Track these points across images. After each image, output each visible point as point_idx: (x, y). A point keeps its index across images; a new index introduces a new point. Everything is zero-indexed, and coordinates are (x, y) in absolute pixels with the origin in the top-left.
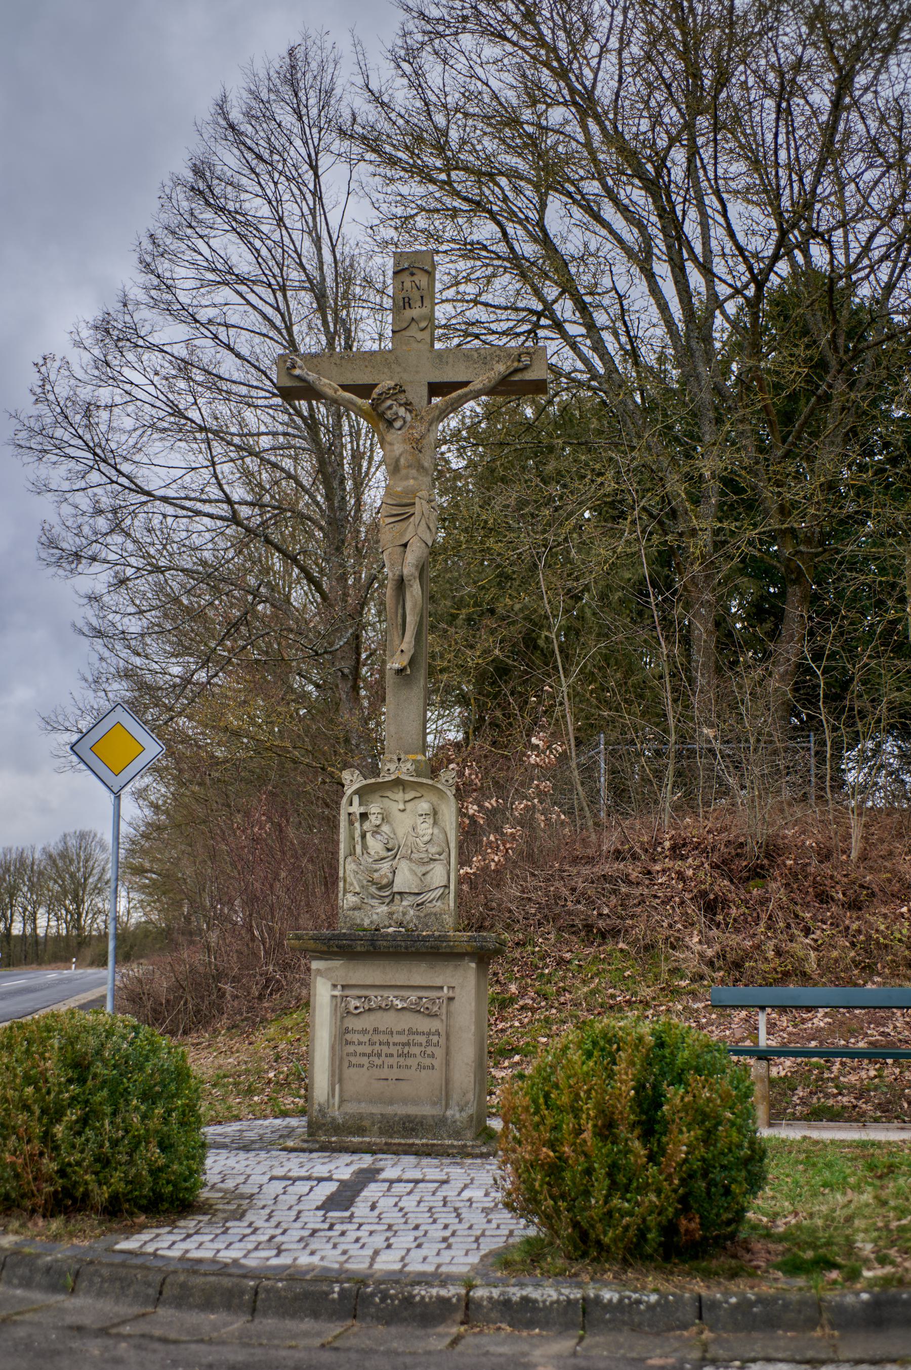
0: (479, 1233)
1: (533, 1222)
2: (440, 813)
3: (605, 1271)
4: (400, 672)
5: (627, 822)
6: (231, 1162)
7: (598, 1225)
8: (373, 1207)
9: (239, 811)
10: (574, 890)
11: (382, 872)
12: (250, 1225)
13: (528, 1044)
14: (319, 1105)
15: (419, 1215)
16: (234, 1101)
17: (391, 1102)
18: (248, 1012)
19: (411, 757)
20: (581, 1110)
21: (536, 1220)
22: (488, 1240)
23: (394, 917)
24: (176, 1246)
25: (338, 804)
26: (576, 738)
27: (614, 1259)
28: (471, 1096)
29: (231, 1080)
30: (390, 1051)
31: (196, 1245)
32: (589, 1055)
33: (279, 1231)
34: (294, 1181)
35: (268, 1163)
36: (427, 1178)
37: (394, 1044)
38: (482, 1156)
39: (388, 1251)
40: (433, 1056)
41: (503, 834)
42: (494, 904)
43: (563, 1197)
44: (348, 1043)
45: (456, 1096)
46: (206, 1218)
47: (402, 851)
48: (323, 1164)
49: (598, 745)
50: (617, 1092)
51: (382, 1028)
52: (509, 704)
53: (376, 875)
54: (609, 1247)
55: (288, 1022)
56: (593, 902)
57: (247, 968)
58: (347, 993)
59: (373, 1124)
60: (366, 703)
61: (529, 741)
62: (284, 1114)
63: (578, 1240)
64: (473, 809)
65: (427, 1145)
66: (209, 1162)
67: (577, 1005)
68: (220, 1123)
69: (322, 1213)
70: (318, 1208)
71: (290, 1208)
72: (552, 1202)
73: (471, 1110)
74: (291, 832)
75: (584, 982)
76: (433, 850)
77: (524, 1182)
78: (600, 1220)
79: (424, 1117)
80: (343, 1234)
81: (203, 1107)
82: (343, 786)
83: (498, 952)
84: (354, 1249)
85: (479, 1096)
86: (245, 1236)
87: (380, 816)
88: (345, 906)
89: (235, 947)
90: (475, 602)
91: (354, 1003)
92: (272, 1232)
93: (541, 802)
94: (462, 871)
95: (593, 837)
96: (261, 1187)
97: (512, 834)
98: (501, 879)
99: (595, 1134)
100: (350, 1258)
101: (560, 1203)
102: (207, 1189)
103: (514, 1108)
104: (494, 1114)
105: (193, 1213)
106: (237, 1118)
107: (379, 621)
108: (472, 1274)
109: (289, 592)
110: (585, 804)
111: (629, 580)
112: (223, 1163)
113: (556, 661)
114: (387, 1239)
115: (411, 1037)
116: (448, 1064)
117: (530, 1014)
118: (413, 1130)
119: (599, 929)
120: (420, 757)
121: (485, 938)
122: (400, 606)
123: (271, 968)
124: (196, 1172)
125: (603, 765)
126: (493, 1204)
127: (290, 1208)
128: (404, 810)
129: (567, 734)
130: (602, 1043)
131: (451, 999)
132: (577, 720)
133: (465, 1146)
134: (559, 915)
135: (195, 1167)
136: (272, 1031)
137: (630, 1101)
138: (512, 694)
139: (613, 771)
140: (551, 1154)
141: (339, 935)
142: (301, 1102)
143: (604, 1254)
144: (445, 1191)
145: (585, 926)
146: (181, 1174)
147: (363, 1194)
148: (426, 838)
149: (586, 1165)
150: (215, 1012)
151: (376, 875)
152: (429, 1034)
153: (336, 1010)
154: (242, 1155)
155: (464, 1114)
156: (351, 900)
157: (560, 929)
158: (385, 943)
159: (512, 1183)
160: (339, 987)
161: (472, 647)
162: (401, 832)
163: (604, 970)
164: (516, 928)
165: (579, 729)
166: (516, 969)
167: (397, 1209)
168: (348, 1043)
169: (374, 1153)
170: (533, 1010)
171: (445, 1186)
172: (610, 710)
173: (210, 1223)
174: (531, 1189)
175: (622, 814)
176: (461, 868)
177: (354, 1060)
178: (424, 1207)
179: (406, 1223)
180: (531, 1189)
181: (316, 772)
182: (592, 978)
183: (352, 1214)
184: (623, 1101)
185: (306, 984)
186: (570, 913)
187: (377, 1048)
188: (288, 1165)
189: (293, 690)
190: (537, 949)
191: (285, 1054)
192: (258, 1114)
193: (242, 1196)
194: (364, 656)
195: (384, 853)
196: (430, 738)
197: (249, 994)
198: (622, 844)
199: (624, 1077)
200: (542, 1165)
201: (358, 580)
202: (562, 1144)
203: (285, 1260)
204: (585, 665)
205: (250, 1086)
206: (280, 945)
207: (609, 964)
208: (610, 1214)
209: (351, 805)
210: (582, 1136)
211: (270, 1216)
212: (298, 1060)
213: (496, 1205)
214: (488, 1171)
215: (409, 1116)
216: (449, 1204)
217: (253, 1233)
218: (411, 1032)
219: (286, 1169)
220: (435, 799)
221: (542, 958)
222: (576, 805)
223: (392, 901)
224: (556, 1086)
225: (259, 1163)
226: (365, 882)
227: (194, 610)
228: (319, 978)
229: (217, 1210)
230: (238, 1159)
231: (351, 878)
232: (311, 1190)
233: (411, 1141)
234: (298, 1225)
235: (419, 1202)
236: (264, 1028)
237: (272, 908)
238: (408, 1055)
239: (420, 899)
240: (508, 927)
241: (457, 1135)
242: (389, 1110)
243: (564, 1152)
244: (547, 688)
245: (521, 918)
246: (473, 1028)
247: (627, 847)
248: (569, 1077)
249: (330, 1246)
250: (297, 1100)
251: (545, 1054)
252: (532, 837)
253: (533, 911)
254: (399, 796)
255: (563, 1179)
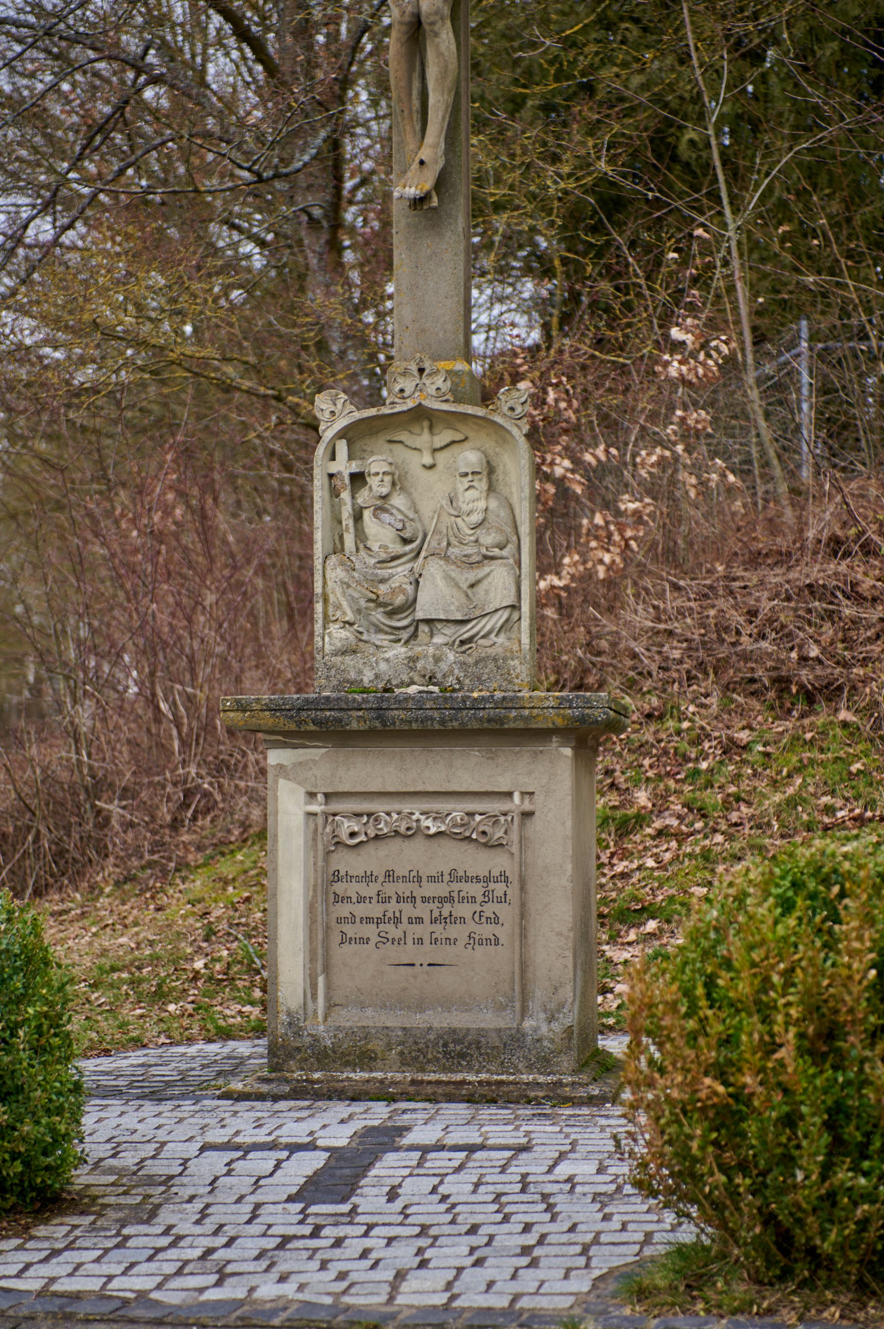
0: (589, 1238)
1: (688, 1216)
2: (500, 471)
3: (826, 1305)
4: (418, 203)
5: (853, 485)
6: (130, 1121)
7: (810, 1219)
8: (392, 1195)
9: (124, 485)
10: (752, 613)
11: (395, 583)
12: (166, 1232)
13: (671, 899)
14: (289, 1014)
15: (478, 1208)
16: (130, 1012)
17: (421, 1008)
18: (152, 852)
19: (443, 365)
20: (775, 1008)
21: (694, 1211)
22: (606, 1250)
23: (419, 665)
24: (31, 1272)
25: (308, 463)
26: (754, 329)
27: (842, 1282)
28: (567, 993)
29: (125, 975)
30: (416, 913)
31: (69, 1269)
32: (787, 906)
33: (221, 1240)
34: (247, 1153)
35: (198, 1120)
36: (490, 1142)
37: (425, 900)
38: (591, 1101)
39: (422, 1273)
40: (495, 920)
41: (618, 513)
42: (604, 644)
43: (743, 1167)
44: (339, 899)
45: (539, 994)
46: (87, 1220)
47: (432, 543)
48: (298, 1120)
49: (793, 344)
50: (845, 972)
51: (401, 872)
52: (628, 265)
53: (383, 589)
54: (830, 1259)
55: (226, 868)
56: (790, 635)
57: (148, 772)
58: (335, 807)
59: (389, 1047)
60: (355, 276)
61: (666, 336)
62: (225, 1035)
63: (774, 1249)
64: (562, 467)
65: (489, 1083)
66: (88, 1121)
67: (762, 826)
68: (107, 1053)
69: (299, 1206)
70: (290, 1199)
71: (239, 1200)
72: (723, 1179)
73: (570, 1018)
74: (221, 520)
75: (774, 784)
76: (488, 539)
77: (670, 1142)
78: (815, 1210)
79: (482, 1032)
80: (338, 1243)
81: (74, 1025)
82: (316, 428)
83: (614, 727)
84: (359, 1270)
85: (584, 994)
86: (158, 1250)
87: (388, 479)
88: (328, 648)
89: (125, 734)
90: (560, 70)
91: (348, 825)
92: (209, 1242)
93: (688, 450)
94: (543, 585)
95: (789, 514)
96: (185, 1162)
97: (636, 512)
98: (616, 597)
99: (801, 1052)
100: (351, 1285)
101: (738, 1180)
102: (87, 1168)
103: (651, 1006)
104: (611, 1028)
105: (62, 1213)
106: (139, 1043)
107: (377, 118)
108: (577, 1311)
109: (203, 66)
110: (772, 453)
111: (856, 18)
112: (114, 1122)
113: (716, 180)
114: (420, 1251)
115: (456, 886)
116: (523, 934)
117: (674, 844)
118: (462, 1055)
119: (802, 686)
120: (460, 366)
121: (588, 700)
122: (416, 76)
123: (193, 770)
124: (66, 1136)
125: (806, 378)
126: (613, 1187)
127: (239, 1200)
128: (432, 467)
129: (737, 322)
130: (812, 885)
131: (527, 815)
132: (756, 295)
133: (559, 1084)
134: (727, 660)
135: (62, 1128)
136: (198, 884)
137: (867, 988)
138: (632, 245)
139: (825, 390)
140: (721, 1089)
141: (316, 701)
142: (255, 1012)
143: (822, 1273)
144: (525, 1164)
145: (775, 681)
146: (37, 1141)
147: (373, 1172)
148: (475, 518)
149: (786, 1109)
150: (93, 855)
151: (383, 589)
152: (487, 879)
153: (314, 840)
154: (149, 1108)
155: (555, 1026)
156: (338, 635)
157: (727, 688)
158: (402, 714)
159: (649, 1144)
160: (320, 797)
161: (555, 159)
162: (427, 508)
163: (812, 761)
164: (647, 685)
165: (759, 313)
166: (647, 762)
167: (437, 1198)
168: (339, 899)
169: (391, 1099)
170: (681, 838)
171: (524, 1156)
172: (819, 273)
173: (93, 1228)
174: (684, 1154)
175: (844, 469)
176: (542, 577)
177: (350, 930)
178: (485, 1193)
179: (453, 1222)
180: (684, 1154)
181: (266, 406)
182: (789, 776)
183: (355, 1207)
184: (856, 989)
185: (259, 799)
186: (746, 657)
187: (392, 907)
188: (234, 1124)
189: (216, 252)
190: (686, 725)
191: (223, 926)
192: (176, 1034)
193: (150, 1181)
194: (349, 184)
195: (397, 548)
196: (477, 340)
197: (153, 818)
198: (844, 525)
199: (856, 945)
200: (703, 1110)
201: (334, 37)
202: (740, 1070)
203: (233, 1291)
204: (770, 189)
205: (159, 986)
206: (208, 728)
207: (822, 750)
208: (831, 1197)
209: (333, 458)
210: (777, 1056)
211: (203, 1215)
212: (249, 936)
213: (619, 1189)
214: (603, 1129)
215: (454, 1031)
216: (532, 1189)
217: (173, 1245)
218: (454, 876)
219: (230, 1131)
220: (489, 444)
221: (696, 742)
222: (755, 455)
223: (414, 635)
224: (727, 964)
225: (180, 1121)
226: (363, 603)
227: (23, 100)
228: (281, 782)
229: (105, 1206)
230: (140, 1115)
231: (336, 595)
232: (277, 1166)
233: (459, 1077)
234: (255, 1229)
235: (477, 1185)
236: (184, 880)
237: (191, 660)
238: (451, 919)
239: (465, 632)
240: (631, 686)
241: (544, 1063)
242: (418, 1021)
243: (744, 1086)
244: (699, 232)
245: (654, 668)
246: (569, 867)
247: (853, 531)
248: (751, 948)
249: (315, 1265)
250: (248, 1008)
251: (705, 907)
252: (675, 517)
253: (677, 654)
254: (423, 439)
255: (743, 1135)
